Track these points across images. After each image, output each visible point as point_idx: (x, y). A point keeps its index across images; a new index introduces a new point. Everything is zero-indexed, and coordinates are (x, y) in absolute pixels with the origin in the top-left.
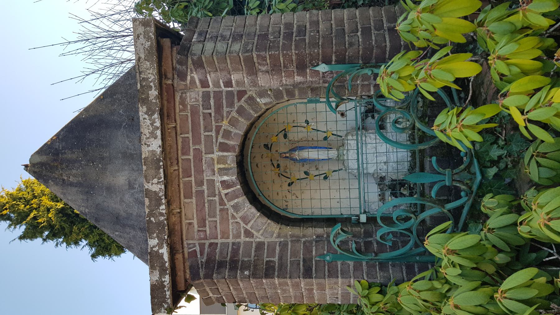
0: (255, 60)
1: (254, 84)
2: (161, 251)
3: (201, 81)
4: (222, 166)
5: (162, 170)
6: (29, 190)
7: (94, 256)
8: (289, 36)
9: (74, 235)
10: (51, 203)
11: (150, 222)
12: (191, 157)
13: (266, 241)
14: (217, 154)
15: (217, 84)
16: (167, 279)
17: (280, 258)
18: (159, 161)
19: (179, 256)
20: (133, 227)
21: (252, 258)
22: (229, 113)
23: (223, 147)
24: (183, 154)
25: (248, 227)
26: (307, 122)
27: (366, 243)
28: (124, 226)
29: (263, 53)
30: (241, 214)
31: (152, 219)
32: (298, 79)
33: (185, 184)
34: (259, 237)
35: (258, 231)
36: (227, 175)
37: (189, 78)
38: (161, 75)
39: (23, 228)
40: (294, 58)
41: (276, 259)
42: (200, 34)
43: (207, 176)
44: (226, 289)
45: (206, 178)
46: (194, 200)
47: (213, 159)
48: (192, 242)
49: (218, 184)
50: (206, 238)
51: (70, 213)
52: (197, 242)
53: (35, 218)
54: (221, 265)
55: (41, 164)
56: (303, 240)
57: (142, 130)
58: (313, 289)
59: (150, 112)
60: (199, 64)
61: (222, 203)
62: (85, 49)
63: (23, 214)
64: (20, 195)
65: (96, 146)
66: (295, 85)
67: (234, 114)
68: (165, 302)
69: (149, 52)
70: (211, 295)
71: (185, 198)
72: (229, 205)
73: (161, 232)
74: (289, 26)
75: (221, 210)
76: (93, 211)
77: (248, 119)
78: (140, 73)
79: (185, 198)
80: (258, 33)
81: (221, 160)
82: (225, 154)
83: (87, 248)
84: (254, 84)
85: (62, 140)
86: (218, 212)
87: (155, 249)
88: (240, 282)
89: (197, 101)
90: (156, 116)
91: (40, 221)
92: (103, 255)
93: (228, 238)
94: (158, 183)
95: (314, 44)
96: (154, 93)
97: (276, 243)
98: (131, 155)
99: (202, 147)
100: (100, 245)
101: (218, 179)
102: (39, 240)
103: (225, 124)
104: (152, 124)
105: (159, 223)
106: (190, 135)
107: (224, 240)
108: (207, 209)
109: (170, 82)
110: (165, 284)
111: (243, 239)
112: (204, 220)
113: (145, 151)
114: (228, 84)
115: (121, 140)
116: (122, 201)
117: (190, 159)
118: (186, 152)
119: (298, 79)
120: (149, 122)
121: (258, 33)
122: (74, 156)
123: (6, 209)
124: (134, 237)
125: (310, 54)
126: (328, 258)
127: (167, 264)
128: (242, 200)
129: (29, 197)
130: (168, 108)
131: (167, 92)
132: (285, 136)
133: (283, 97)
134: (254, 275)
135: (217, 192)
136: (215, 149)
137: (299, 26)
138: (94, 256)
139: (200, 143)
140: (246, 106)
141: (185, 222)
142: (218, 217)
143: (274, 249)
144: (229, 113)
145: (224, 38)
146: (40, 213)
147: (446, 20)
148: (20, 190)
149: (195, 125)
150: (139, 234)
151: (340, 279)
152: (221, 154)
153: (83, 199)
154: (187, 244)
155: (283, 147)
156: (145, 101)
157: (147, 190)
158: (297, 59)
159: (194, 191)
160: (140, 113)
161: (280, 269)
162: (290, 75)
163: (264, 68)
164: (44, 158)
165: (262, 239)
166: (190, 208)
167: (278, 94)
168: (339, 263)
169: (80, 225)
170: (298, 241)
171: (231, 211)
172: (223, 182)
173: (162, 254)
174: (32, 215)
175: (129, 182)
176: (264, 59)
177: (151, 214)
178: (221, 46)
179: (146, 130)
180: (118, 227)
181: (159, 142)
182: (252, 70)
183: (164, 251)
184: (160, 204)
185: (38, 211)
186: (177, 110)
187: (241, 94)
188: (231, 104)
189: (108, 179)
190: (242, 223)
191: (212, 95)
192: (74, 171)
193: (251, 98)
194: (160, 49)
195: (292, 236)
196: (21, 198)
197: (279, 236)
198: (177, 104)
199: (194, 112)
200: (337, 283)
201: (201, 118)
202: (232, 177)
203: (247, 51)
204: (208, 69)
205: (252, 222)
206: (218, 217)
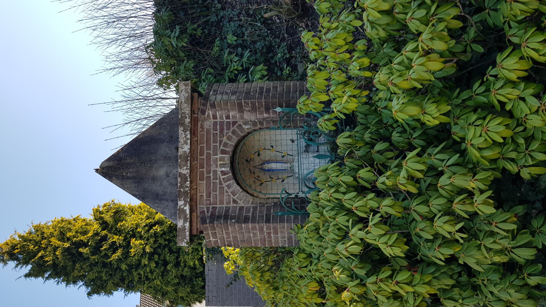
0: (243, 104)
1: (242, 118)
2: (185, 208)
3: (213, 115)
4: (222, 162)
5: (189, 162)
6: (39, 233)
7: (89, 294)
8: (261, 93)
9: (76, 271)
10: (59, 242)
11: (180, 191)
12: (205, 157)
13: (245, 206)
14: (219, 156)
15: (221, 117)
16: (187, 224)
17: (253, 214)
18: (188, 157)
19: (194, 214)
20: (167, 200)
21: (237, 214)
22: (227, 133)
23: (223, 152)
24: (200, 155)
25: (235, 198)
26: (272, 147)
27: (301, 207)
28: (161, 200)
29: (247, 101)
30: (231, 190)
31: (182, 190)
32: (266, 115)
33: (200, 172)
34: (241, 204)
35: (241, 200)
36: (224, 167)
37: (207, 113)
38: (192, 112)
39: (29, 267)
40: (263, 103)
41: (250, 214)
42: (214, 91)
43: (213, 168)
44: (221, 233)
45: (212, 169)
46: (205, 182)
47: (217, 159)
48: (202, 206)
49: (219, 173)
50: (210, 204)
51: (75, 252)
52: (205, 207)
53: (42, 257)
54: (219, 217)
55: (108, 167)
56: (266, 205)
57: (180, 140)
58: (271, 233)
59: (185, 131)
60: (213, 106)
61: (221, 184)
62: (124, 108)
63: (31, 254)
64: (30, 237)
65: (148, 154)
66: (264, 119)
67: (230, 134)
68: (185, 238)
69: (187, 99)
70: (211, 239)
71: (200, 180)
72: (224, 185)
73: (186, 197)
74: (261, 88)
75: (220, 188)
76: (141, 193)
77: (238, 137)
78: (181, 110)
79: (200, 180)
80: (245, 91)
81: (222, 159)
82: (224, 156)
83: (84, 288)
84: (242, 118)
85: (125, 152)
86: (218, 189)
87: (182, 207)
88: (229, 227)
89: (210, 126)
90: (188, 132)
91: (47, 259)
92: (98, 293)
93: (223, 204)
94: (187, 169)
95: (274, 96)
96: (188, 120)
97: (250, 207)
98: (170, 157)
99: (211, 152)
100: (96, 284)
101: (219, 169)
102: (40, 279)
103: (225, 139)
104: (185, 137)
105: (186, 192)
106: (205, 145)
107: (221, 206)
108: (212, 187)
109: (196, 116)
110: (186, 227)
111: (232, 204)
112: (210, 194)
113: (181, 152)
114: (228, 117)
115: (164, 149)
116: (161, 185)
117: (204, 159)
118: (202, 155)
119: (266, 115)
120: (184, 136)
121: (245, 91)
122: (132, 161)
123: (17, 249)
124: (167, 206)
125: (272, 102)
126: (280, 214)
127: (188, 216)
128: (232, 182)
129: (38, 239)
130: (194, 130)
131: (194, 121)
132: (259, 155)
133: (257, 125)
134: (238, 222)
135: (218, 177)
136: (219, 152)
137: (266, 89)
138: (89, 294)
139: (210, 150)
140: (237, 130)
141: (199, 194)
142: (218, 192)
143: (249, 210)
144: (227, 133)
145: (227, 93)
146: (47, 253)
147: (317, 80)
148: (30, 233)
149: (208, 140)
150: (171, 204)
151: (286, 224)
152: (221, 155)
153: (135, 187)
154: (200, 207)
155: (257, 161)
156: (183, 124)
157: (180, 173)
158: (265, 104)
159: (205, 176)
160: (180, 131)
161: (252, 219)
162: (261, 113)
163: (247, 109)
164: (111, 163)
165: (243, 205)
166: (202, 186)
167: (254, 123)
168: (286, 216)
169: (82, 263)
170: (263, 206)
171: (226, 188)
172: (222, 172)
173: (186, 210)
174: (40, 254)
175: (167, 173)
176: (248, 104)
177: (181, 187)
178: (225, 97)
179: (181, 140)
180: (157, 201)
181: (189, 147)
182: (241, 110)
183: (187, 208)
184: (187, 181)
185: (46, 252)
186: (199, 131)
187: (234, 123)
188: (228, 129)
189: (154, 173)
190: (231, 195)
191: (218, 123)
192: (131, 170)
193: (240, 125)
194: (192, 98)
195: (260, 203)
196: (30, 240)
197: (252, 203)
198: (199, 128)
199: (208, 132)
200: (284, 227)
201: (212, 136)
202: (227, 169)
203: (239, 100)
204: (217, 109)
205: (237, 195)
206: (218, 192)
